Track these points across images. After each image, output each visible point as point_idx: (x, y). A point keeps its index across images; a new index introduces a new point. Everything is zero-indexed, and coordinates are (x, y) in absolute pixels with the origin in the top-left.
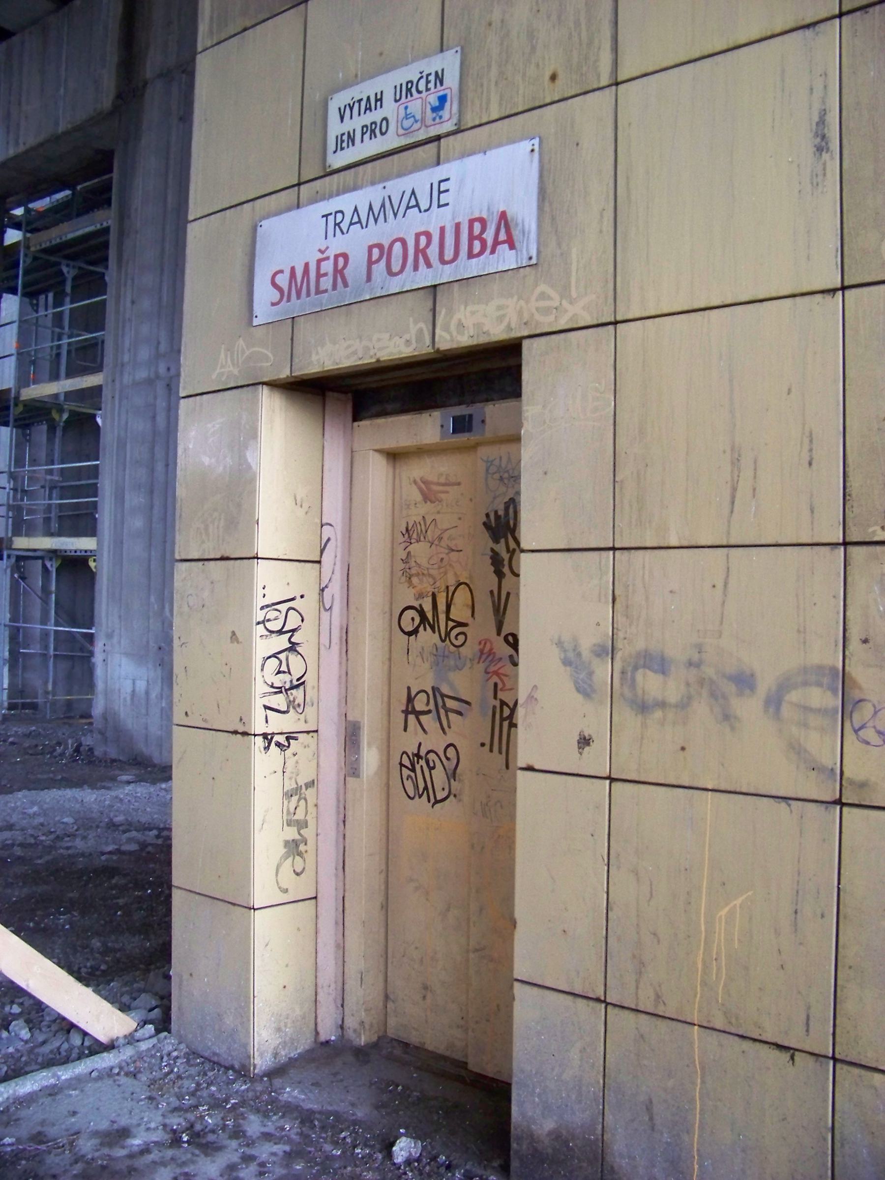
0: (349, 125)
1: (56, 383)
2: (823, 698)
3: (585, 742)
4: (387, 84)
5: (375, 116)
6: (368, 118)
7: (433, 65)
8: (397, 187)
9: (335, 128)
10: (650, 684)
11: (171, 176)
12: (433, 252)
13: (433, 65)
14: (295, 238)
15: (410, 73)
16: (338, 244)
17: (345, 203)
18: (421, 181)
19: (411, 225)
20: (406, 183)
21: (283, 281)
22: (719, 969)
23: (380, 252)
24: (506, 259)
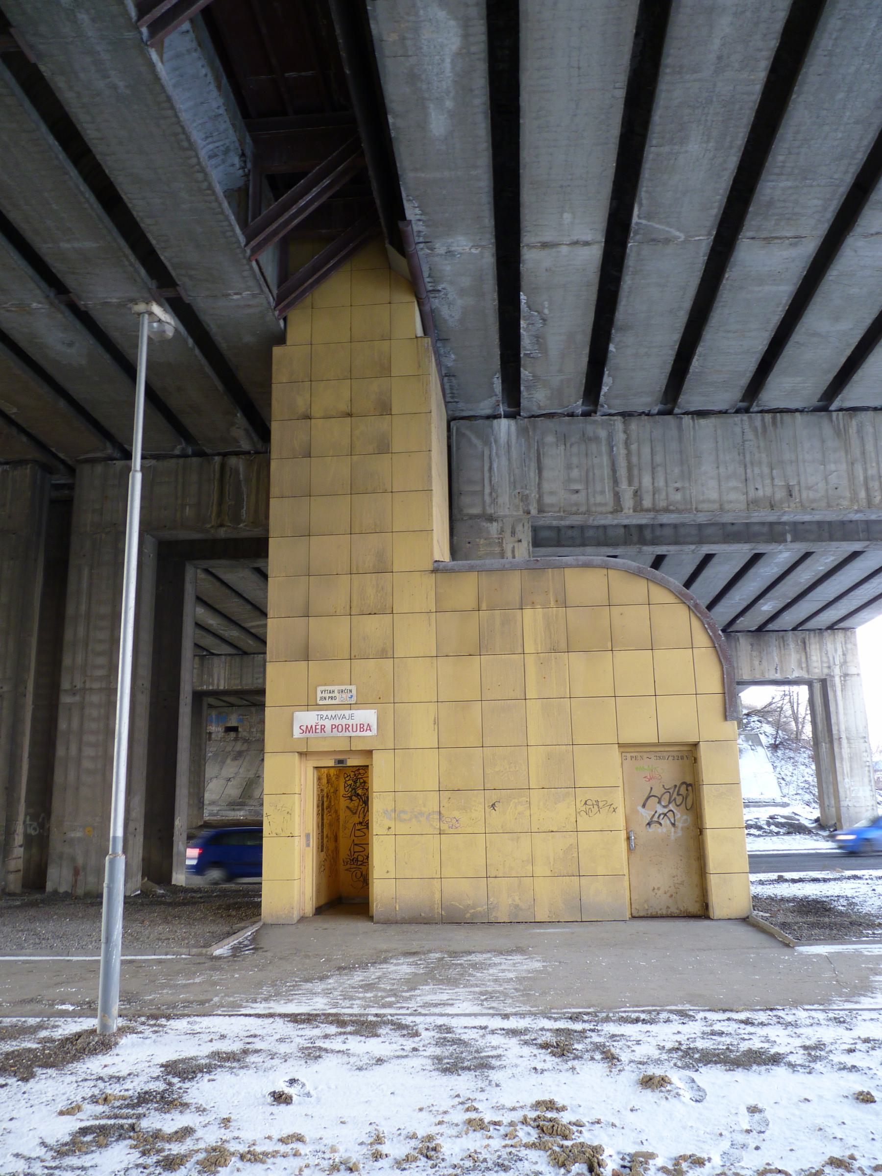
0: (323, 695)
1: (199, 877)
2: (437, 816)
3: (389, 828)
4: (336, 688)
5: (333, 695)
6: (330, 695)
7: (349, 687)
8: (339, 713)
9: (319, 695)
10: (403, 816)
11: (862, 478)
12: (350, 729)
13: (349, 687)
14: (305, 718)
15: (343, 687)
16: (321, 722)
17: (324, 713)
18: (347, 713)
19: (344, 722)
20: (343, 712)
21: (304, 728)
22: (300, 780)
23: (334, 727)
24: (368, 733)
